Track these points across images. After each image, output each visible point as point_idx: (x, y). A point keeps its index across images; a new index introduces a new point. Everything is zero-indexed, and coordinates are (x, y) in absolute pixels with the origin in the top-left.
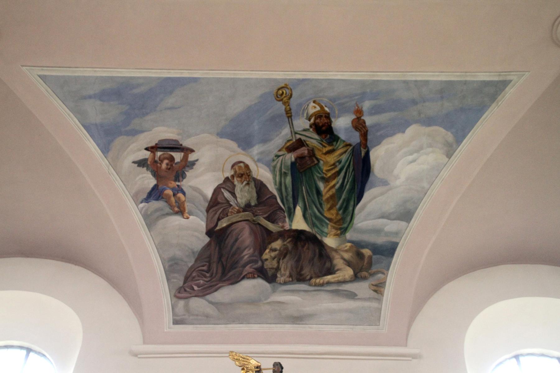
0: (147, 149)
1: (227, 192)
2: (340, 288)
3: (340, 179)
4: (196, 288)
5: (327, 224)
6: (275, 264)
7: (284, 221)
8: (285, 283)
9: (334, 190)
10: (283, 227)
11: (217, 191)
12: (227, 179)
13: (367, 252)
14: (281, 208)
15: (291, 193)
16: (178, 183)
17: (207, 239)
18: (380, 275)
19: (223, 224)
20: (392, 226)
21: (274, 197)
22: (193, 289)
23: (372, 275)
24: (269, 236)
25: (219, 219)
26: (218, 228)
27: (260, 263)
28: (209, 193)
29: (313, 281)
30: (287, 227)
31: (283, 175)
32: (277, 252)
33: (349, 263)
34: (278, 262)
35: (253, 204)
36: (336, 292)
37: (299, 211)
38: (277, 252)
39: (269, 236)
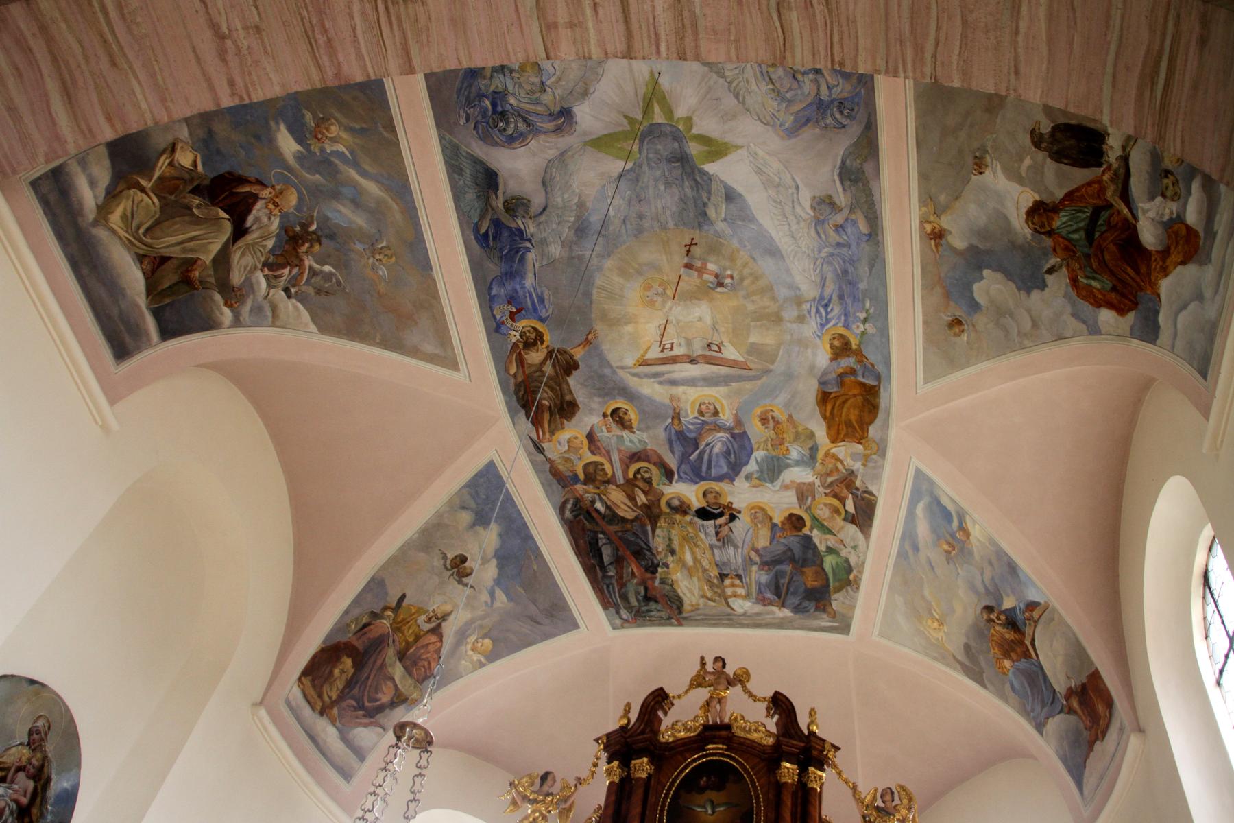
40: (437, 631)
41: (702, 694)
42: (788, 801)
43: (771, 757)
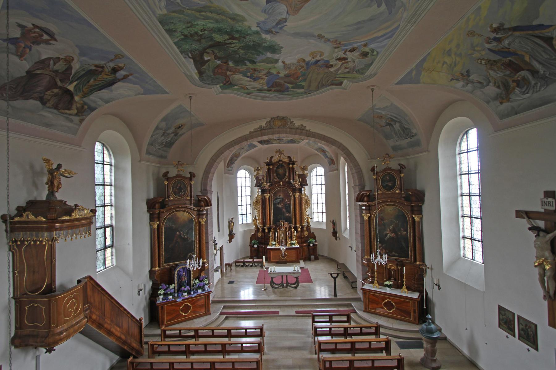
0: (33, 25)
1: (53, 62)
2: (69, 117)
3: (100, 82)
4: (5, 95)
5: (81, 92)
6: (49, 97)
7: (66, 84)
8: (49, 107)
9: (94, 84)
10: (64, 85)
11: (49, 59)
12: (59, 58)
13: (86, 107)
14: (69, 79)
15: (78, 76)
16: (31, 45)
17: (25, 74)
18: (85, 117)
19: (39, 72)
20: (100, 102)
21: (71, 74)
22: (3, 95)
23: (82, 115)
24: (55, 86)
25: (38, 69)
26: (34, 72)
27: (42, 95)
28: (44, 57)
29: (61, 110)
30: (65, 86)
31: (83, 70)
32: (53, 93)
33: (77, 109)
34: (51, 97)
35: (59, 72)
36: (67, 118)
37: (75, 83)
38: (53, 93)
39: (55, 86)
40: (240, 153)
41: (278, 154)
42: (291, 170)
43: (289, 164)
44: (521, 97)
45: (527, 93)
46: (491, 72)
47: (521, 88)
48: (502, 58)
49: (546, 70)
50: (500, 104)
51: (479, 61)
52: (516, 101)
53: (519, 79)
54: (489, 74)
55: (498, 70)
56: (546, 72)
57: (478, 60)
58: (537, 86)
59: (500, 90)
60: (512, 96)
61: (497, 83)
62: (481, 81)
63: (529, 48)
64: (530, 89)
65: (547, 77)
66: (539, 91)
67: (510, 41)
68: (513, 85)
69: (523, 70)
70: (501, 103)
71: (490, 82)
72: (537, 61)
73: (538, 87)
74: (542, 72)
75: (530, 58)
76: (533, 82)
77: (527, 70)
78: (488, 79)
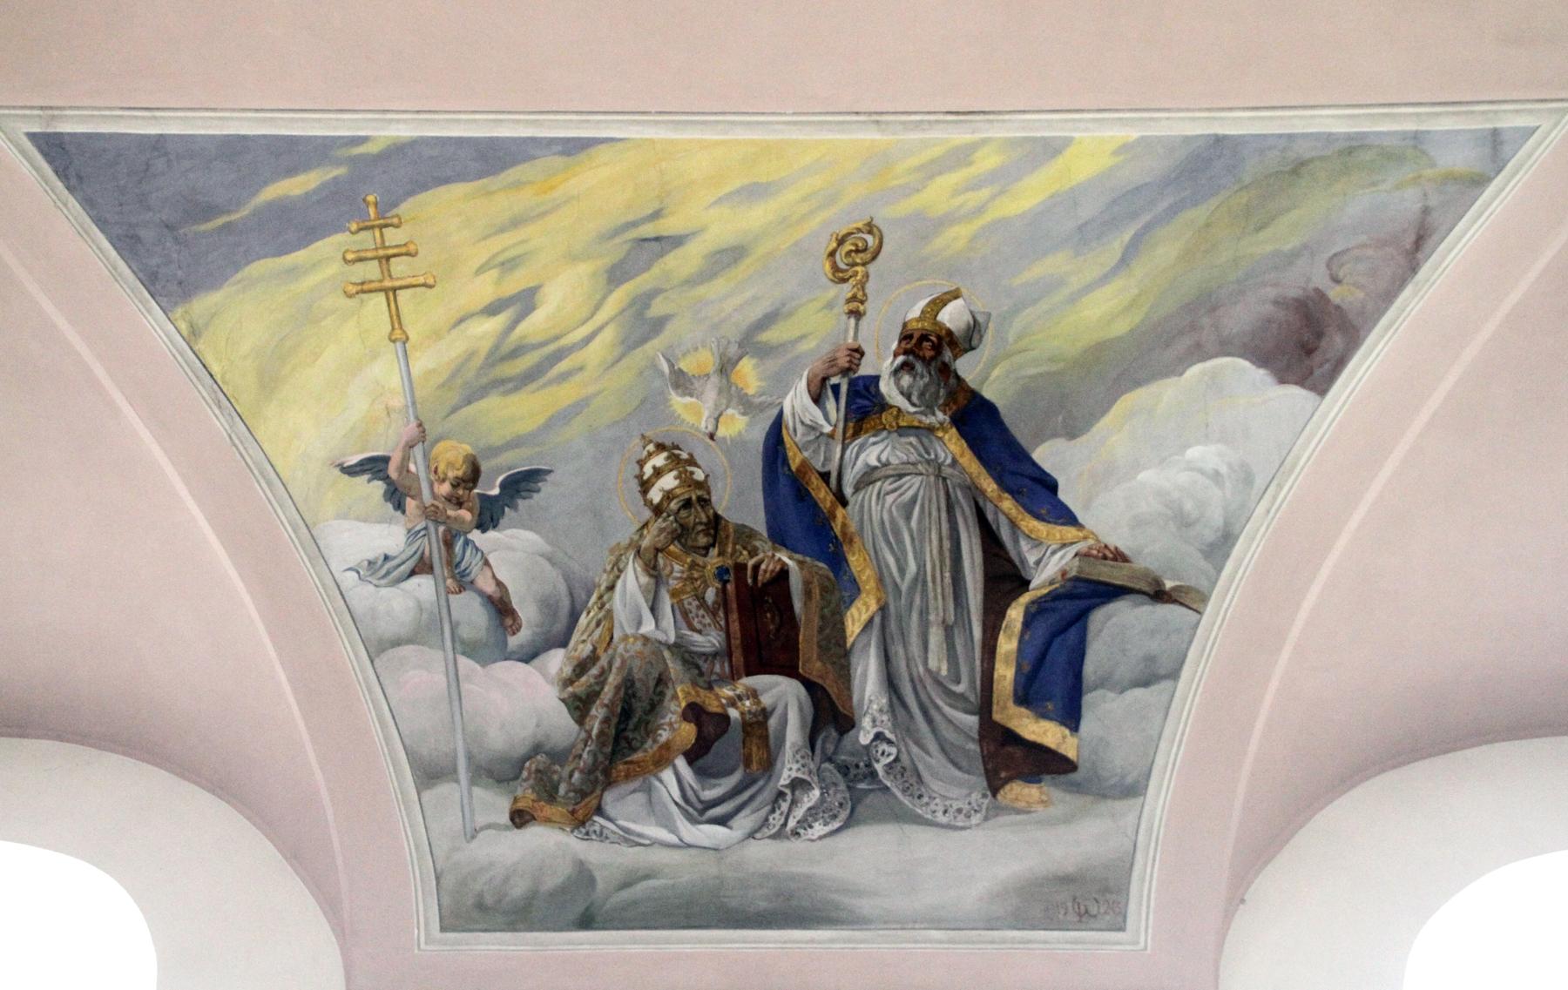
44: (674, 831)
45: (723, 821)
46: (633, 579)
47: (703, 773)
48: (765, 534)
49: (889, 735)
50: (505, 818)
51: (660, 460)
52: (629, 839)
53: (734, 713)
54: (611, 588)
55: (674, 594)
56: (884, 747)
57: (661, 447)
58: (794, 803)
59: (575, 727)
60: (623, 806)
61: (594, 671)
62: (515, 604)
63: (912, 567)
64: (752, 798)
65: (873, 775)
66: (796, 834)
67: (886, 464)
68: (675, 729)
69: (790, 671)
70: (520, 818)
71: (563, 643)
72: (886, 658)
73: (799, 813)
74: (865, 738)
75: (869, 624)
76: (789, 769)
77: (809, 685)
78: (574, 617)
